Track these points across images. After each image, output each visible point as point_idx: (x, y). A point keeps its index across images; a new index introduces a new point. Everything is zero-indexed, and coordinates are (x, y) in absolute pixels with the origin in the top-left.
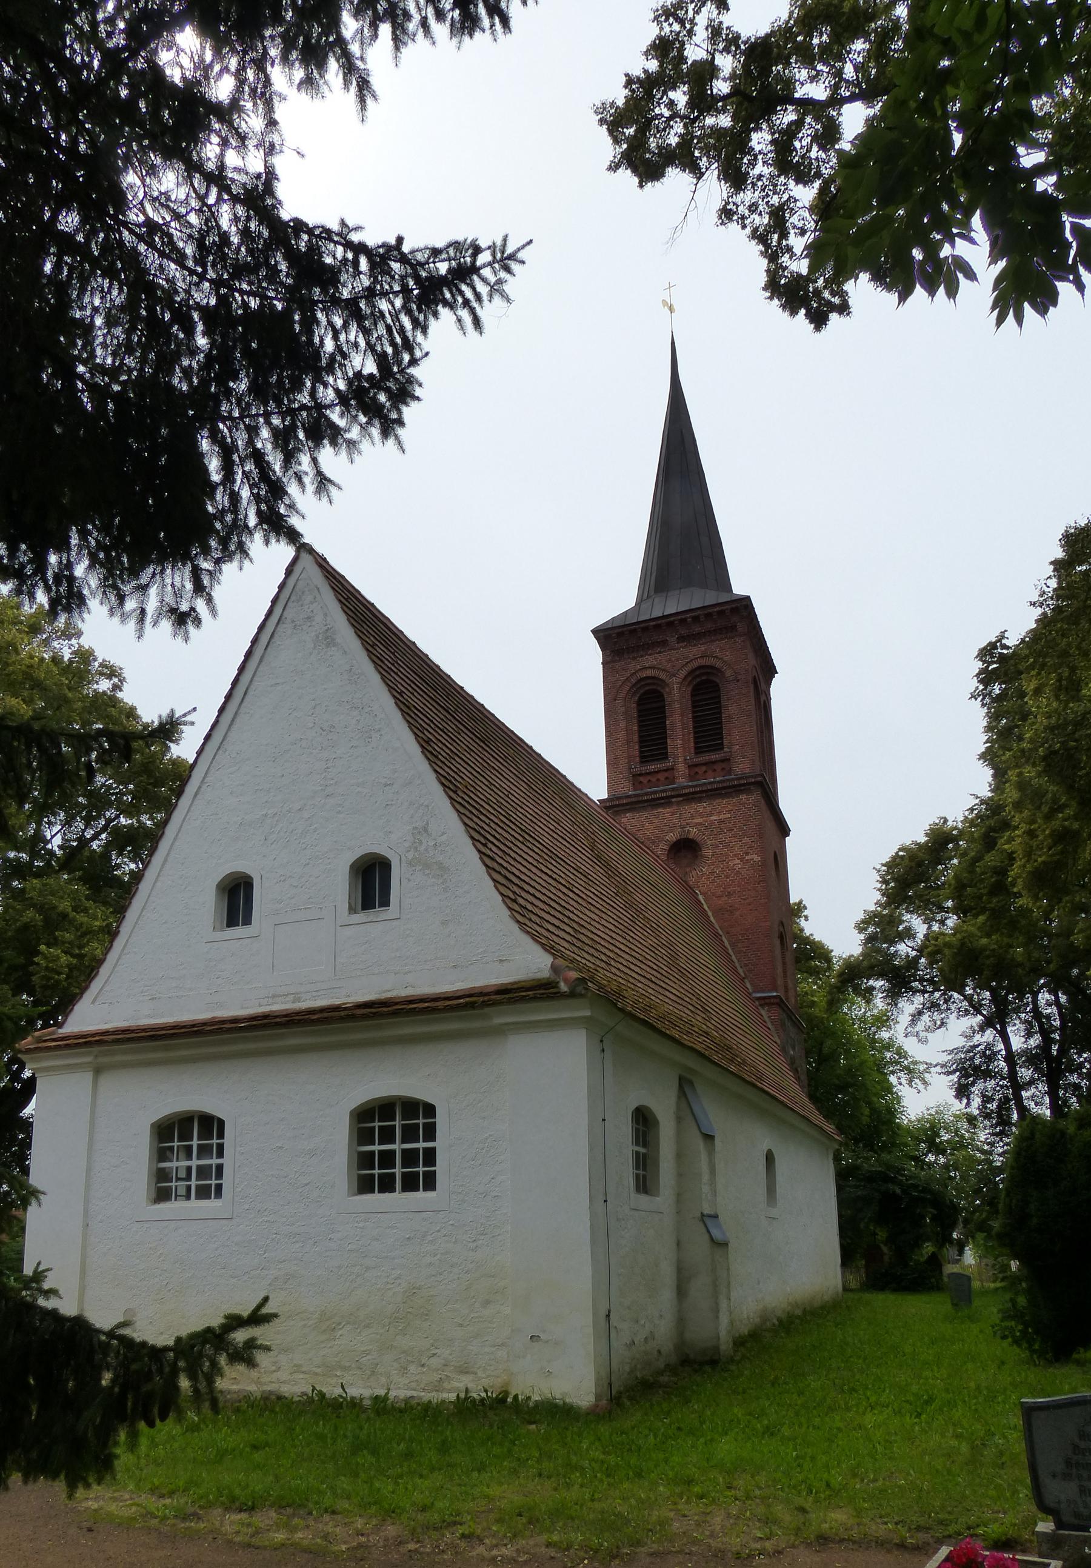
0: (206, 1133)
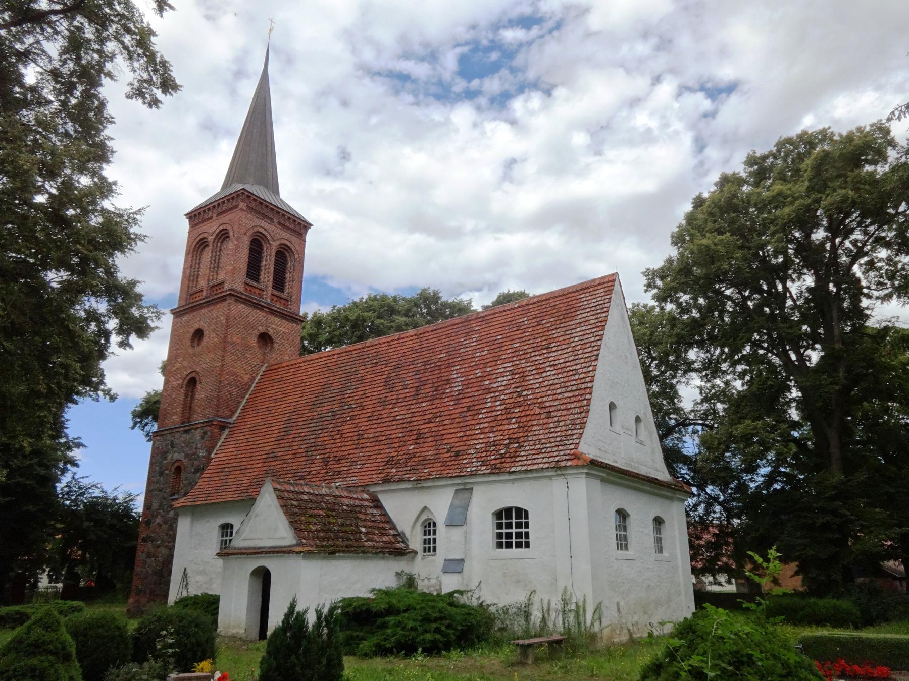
0: (518, 516)
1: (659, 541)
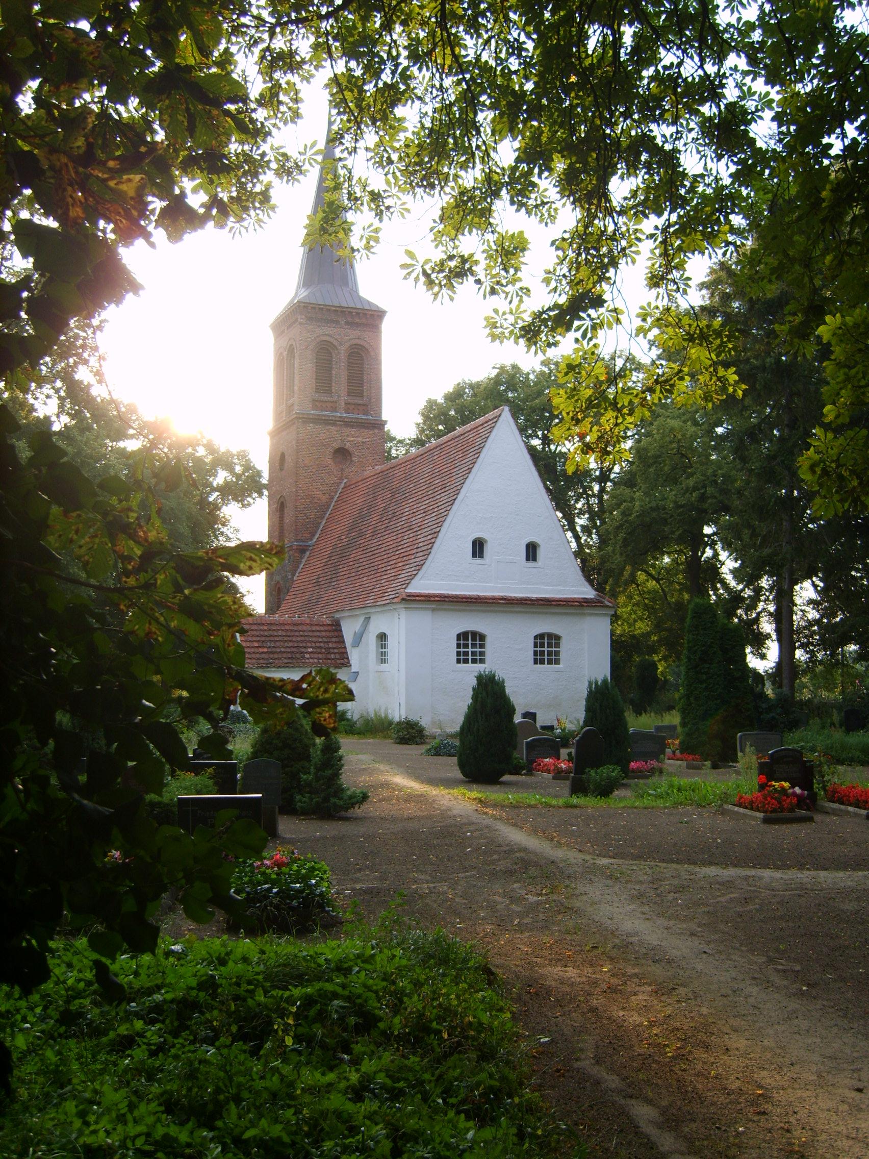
1: (383, 654)
